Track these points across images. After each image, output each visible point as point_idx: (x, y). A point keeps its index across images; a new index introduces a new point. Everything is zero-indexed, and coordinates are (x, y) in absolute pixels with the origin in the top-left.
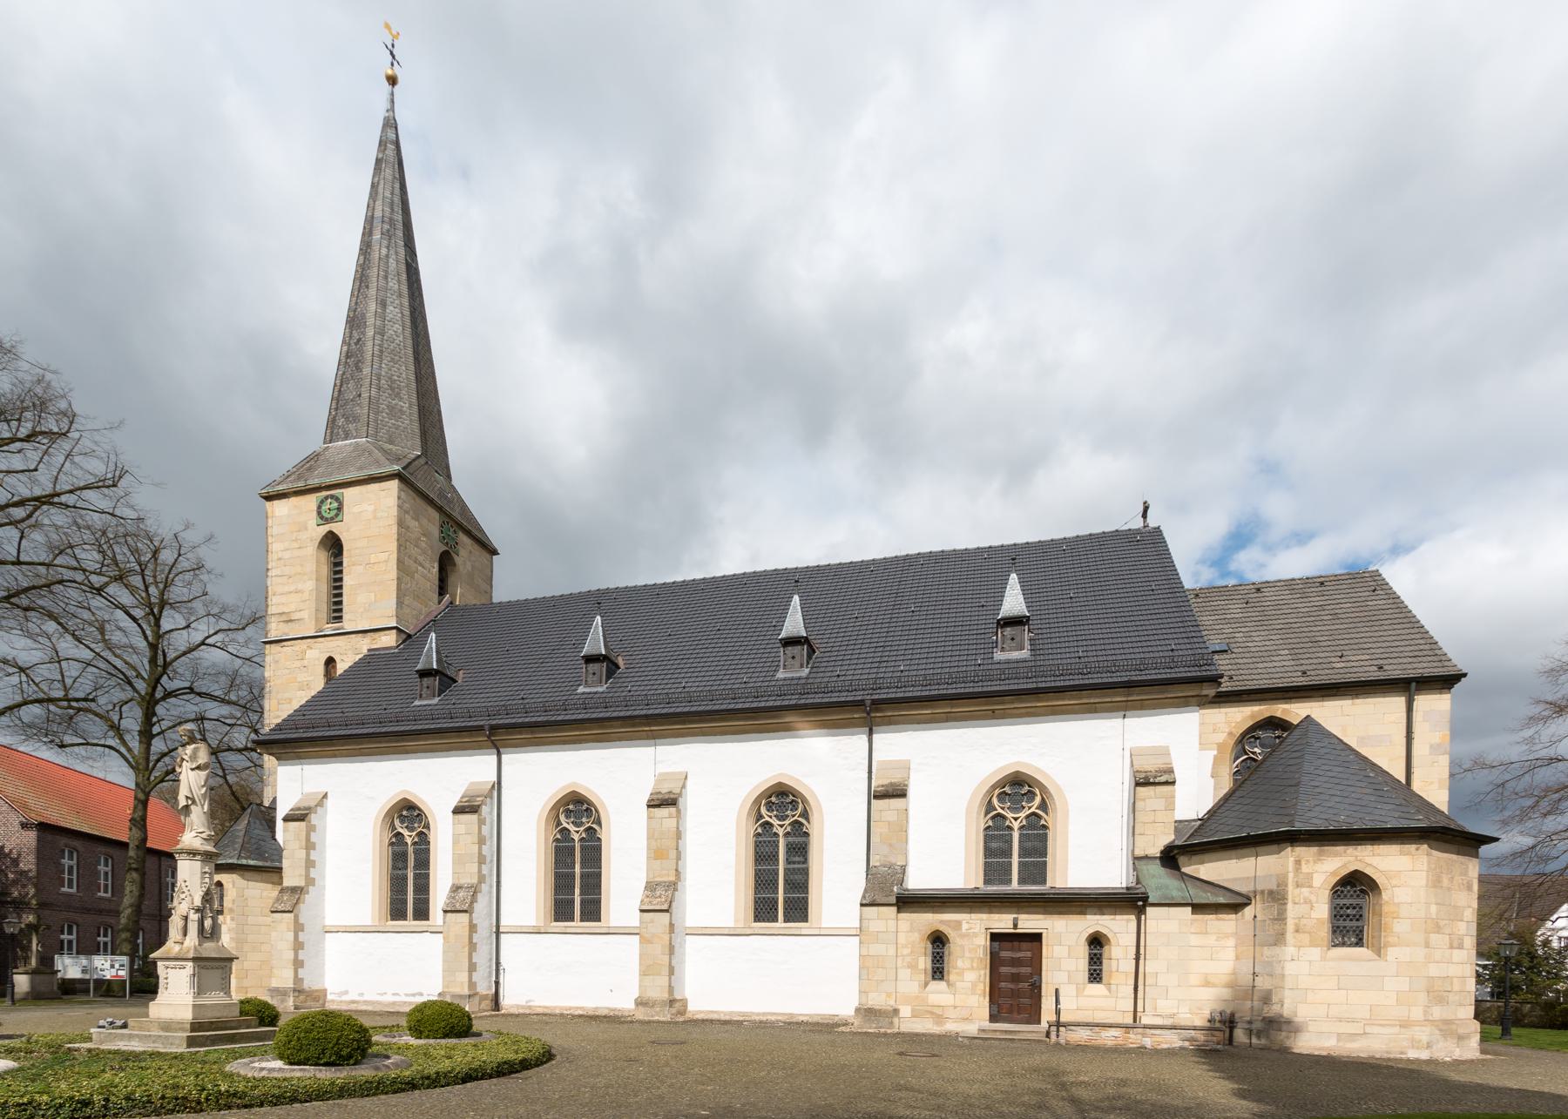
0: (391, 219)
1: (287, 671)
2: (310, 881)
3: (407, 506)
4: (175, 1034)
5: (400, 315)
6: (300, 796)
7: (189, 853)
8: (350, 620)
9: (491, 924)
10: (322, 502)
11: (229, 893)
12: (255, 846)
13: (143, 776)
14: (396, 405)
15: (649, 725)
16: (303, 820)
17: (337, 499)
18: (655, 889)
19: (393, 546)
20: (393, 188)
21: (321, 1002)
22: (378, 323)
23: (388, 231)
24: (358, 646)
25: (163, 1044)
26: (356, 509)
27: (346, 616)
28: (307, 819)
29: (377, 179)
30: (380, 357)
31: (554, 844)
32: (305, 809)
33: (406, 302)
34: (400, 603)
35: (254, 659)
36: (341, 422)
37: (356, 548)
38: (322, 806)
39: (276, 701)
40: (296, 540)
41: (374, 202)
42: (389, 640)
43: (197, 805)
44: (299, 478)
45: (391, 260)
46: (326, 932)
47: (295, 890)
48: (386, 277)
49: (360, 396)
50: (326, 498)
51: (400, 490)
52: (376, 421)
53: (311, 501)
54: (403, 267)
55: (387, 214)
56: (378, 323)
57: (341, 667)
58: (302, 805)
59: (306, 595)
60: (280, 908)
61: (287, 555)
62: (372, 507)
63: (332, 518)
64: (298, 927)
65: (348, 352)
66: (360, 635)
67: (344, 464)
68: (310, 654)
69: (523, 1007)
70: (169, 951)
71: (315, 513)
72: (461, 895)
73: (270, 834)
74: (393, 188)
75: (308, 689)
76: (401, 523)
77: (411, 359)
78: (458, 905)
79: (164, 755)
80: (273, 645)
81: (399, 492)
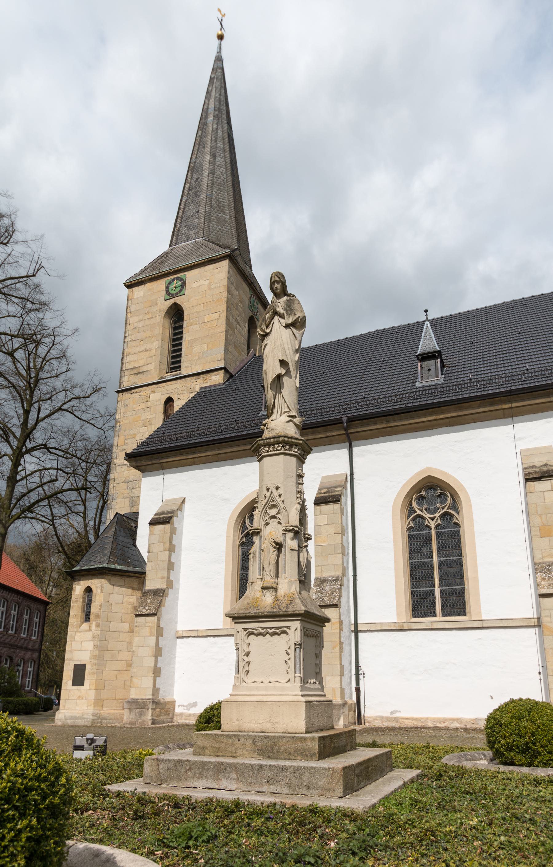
0: (219, 109)
1: (135, 412)
2: (170, 584)
3: (232, 279)
4: (288, 763)
5: (224, 162)
6: (160, 504)
7: (286, 443)
8: (187, 367)
9: (350, 621)
10: (170, 283)
11: (97, 598)
12: (120, 552)
13: (6, 514)
14: (222, 217)
15: (511, 402)
16: (168, 522)
17: (181, 279)
18: (549, 570)
19: (224, 307)
20: (220, 92)
21: (171, 716)
22: (211, 167)
23: (218, 115)
24: (191, 387)
25: (290, 786)
26: (195, 285)
27: (183, 365)
28: (171, 521)
29: (210, 88)
30: (212, 187)
31: (408, 533)
32: (169, 512)
33: (228, 155)
34: (226, 350)
35: (91, 422)
36: (184, 230)
37: (195, 312)
38: (181, 511)
39: (123, 437)
40: (148, 313)
41: (209, 101)
42: (218, 379)
43: (291, 377)
44: (154, 270)
45: (219, 131)
46: (177, 637)
47: (159, 593)
48: (216, 141)
49: (198, 212)
50: (173, 280)
51: (229, 267)
52: (209, 226)
53: (161, 284)
54: (226, 135)
55: (217, 106)
56: (211, 167)
57: (178, 405)
58: (165, 510)
59: (153, 352)
60: (144, 611)
61: (140, 324)
62: (208, 282)
63: (177, 294)
64: (160, 632)
65: (189, 188)
66: (194, 377)
67: (188, 255)
68: (153, 397)
69: (388, 719)
70: (255, 603)
71: (164, 292)
72: (327, 588)
73: (130, 541)
74: (220, 92)
75: (150, 424)
76: (229, 291)
77: (231, 189)
78: (326, 599)
79: (24, 495)
80: (124, 394)
81: (229, 269)
